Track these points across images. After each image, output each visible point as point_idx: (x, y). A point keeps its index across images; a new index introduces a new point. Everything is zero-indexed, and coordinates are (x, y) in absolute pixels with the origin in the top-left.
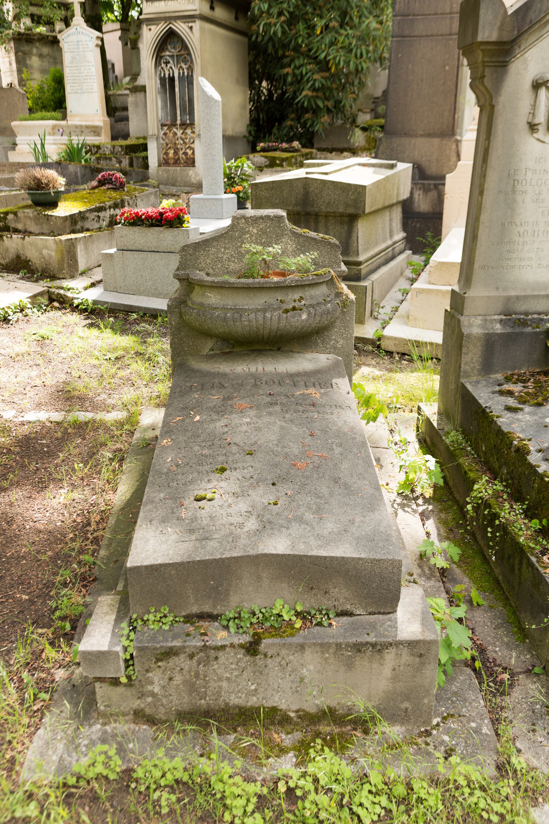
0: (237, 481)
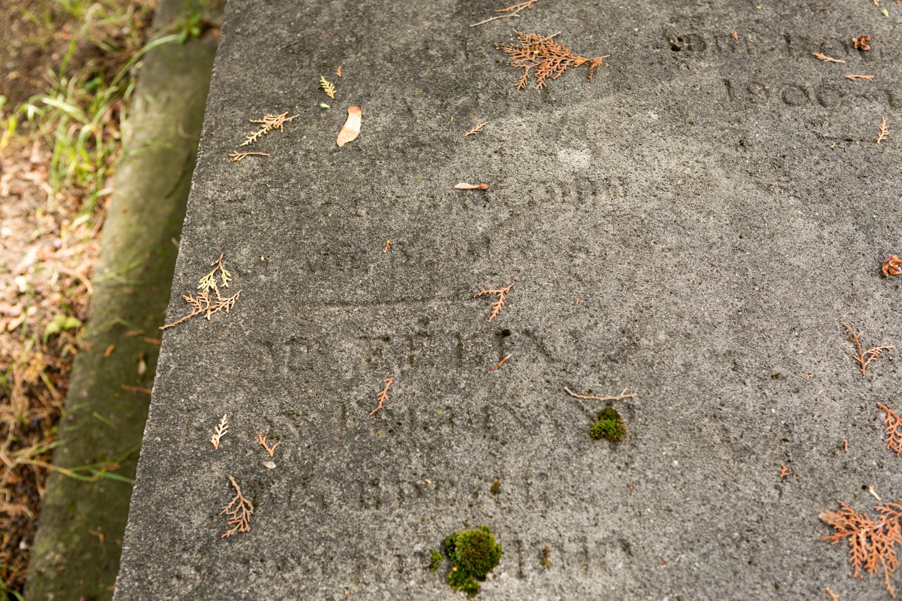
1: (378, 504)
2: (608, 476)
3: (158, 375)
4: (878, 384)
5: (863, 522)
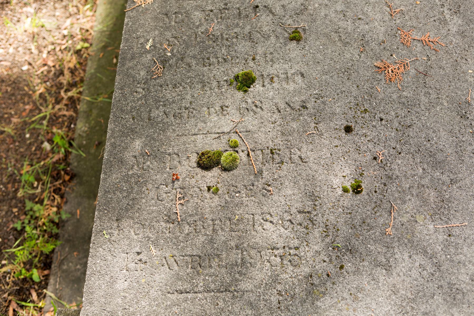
0: (276, 116)
1: (210, 65)
2: (296, 52)
3: (125, 27)
4: (398, 21)
5: (390, 66)
